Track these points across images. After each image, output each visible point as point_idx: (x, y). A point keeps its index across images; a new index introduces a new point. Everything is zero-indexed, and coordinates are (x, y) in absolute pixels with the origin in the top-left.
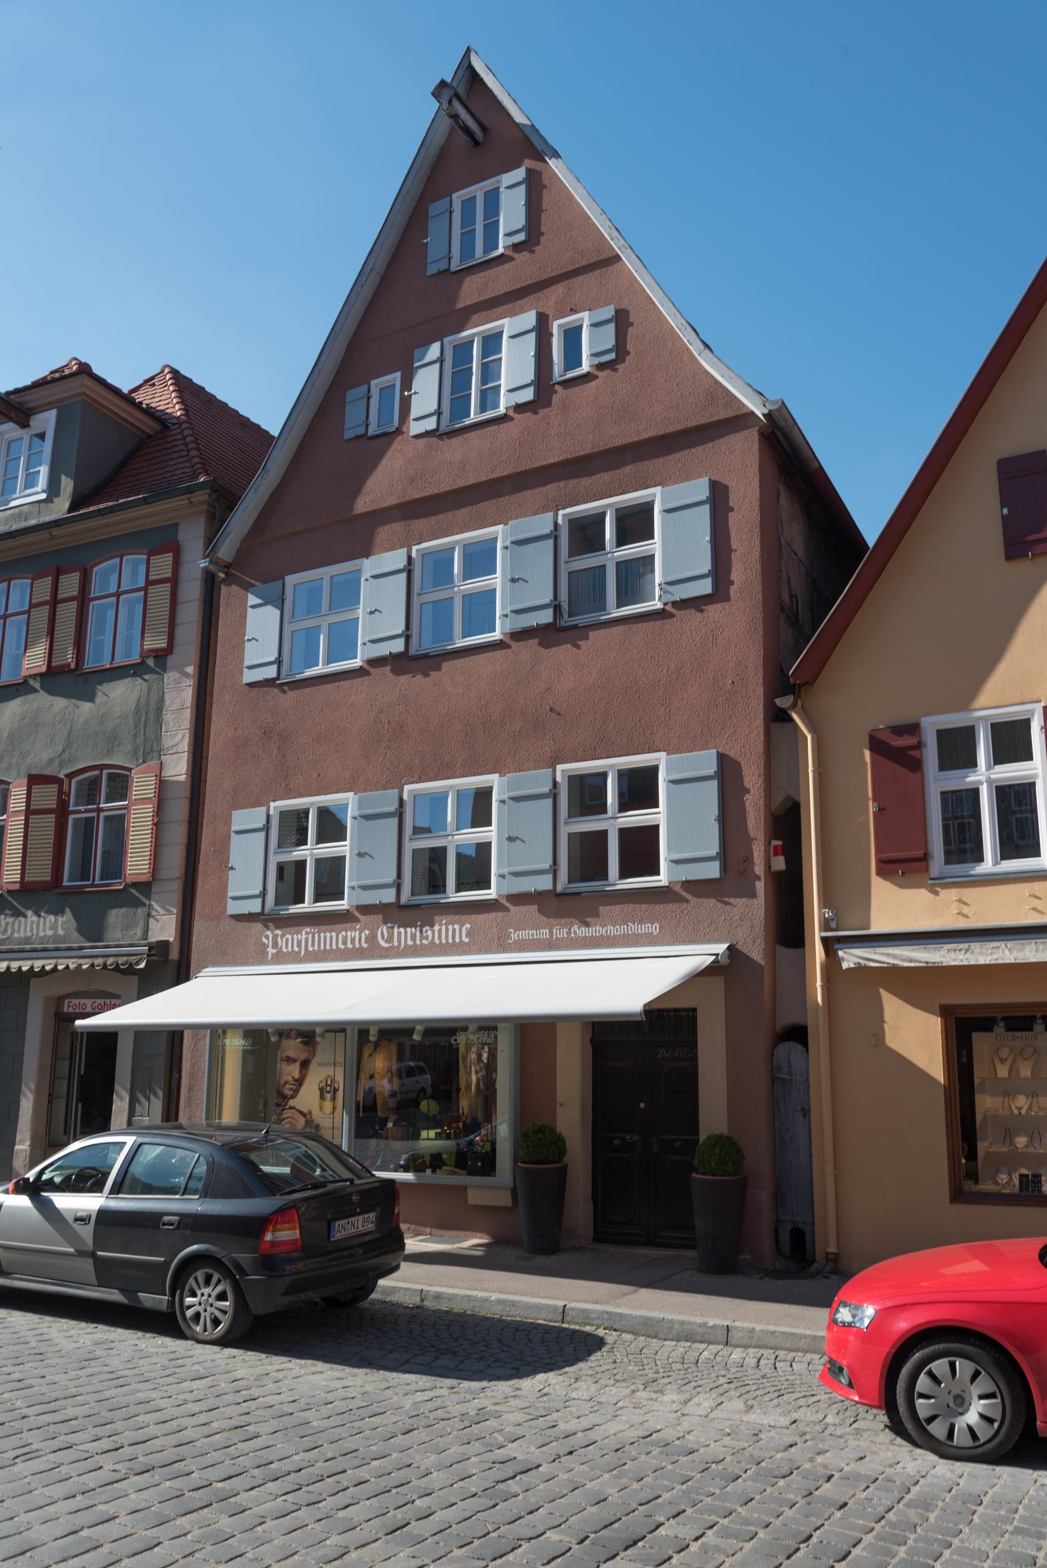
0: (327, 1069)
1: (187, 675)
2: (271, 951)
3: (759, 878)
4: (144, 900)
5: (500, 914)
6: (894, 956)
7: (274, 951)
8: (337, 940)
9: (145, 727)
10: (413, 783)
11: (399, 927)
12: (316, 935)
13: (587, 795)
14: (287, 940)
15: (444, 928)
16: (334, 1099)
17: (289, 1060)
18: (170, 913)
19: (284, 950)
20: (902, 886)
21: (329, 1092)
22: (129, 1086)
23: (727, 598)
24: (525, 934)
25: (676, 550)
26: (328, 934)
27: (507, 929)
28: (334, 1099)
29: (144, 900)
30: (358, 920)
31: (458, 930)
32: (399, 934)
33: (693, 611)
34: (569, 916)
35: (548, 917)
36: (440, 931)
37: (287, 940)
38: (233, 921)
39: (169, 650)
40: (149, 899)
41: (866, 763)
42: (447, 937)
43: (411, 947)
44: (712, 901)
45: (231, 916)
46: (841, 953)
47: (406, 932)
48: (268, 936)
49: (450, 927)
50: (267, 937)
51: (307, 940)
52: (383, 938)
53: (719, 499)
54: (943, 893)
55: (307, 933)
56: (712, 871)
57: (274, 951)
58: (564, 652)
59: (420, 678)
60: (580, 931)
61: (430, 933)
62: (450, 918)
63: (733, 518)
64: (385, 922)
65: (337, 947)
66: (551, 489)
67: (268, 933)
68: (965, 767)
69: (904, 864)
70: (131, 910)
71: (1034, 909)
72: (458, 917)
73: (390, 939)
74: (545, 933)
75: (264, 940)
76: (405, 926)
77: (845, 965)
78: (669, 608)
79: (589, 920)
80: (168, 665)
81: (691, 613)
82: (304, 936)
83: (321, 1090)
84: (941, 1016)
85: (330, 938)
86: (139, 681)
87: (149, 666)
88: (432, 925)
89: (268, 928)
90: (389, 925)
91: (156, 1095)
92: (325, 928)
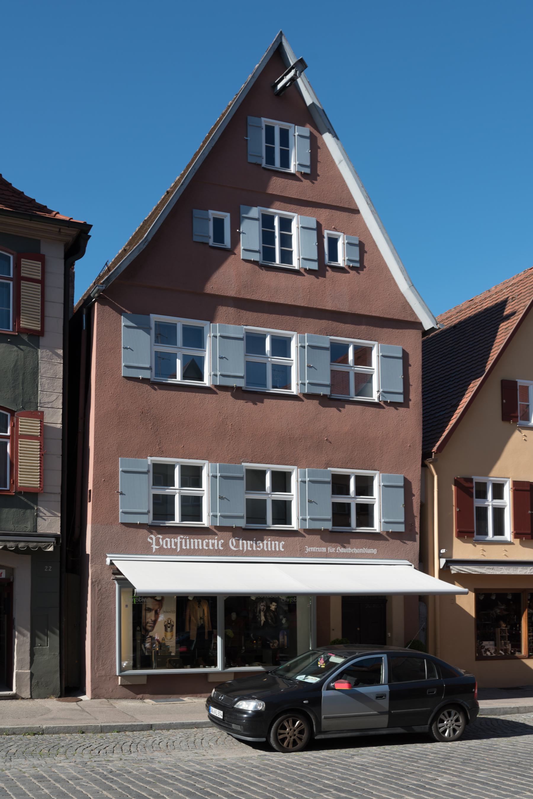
0: (166, 616)
1: (58, 355)
2: (154, 547)
3: (417, 533)
4: (32, 505)
5: (301, 538)
6: (469, 570)
7: (157, 547)
8: (202, 544)
9: (23, 384)
10: (248, 462)
11: (242, 540)
12: (188, 540)
13: (255, 479)
14: (167, 541)
15: (269, 543)
16: (172, 631)
17: (150, 610)
18: (56, 516)
19: (165, 546)
20: (464, 542)
21: (169, 627)
22: (29, 627)
23: (408, 407)
24: (314, 549)
25: (380, 376)
26: (196, 540)
27: (304, 546)
28: (172, 631)
29: (32, 505)
30: (216, 534)
31: (279, 545)
32: (243, 544)
33: (393, 408)
34: (336, 542)
35: (326, 542)
36: (267, 544)
37: (167, 541)
38: (124, 527)
39: (41, 333)
40: (37, 505)
41: (452, 491)
42: (271, 547)
43: (250, 551)
44: (399, 541)
45: (122, 523)
46: (451, 567)
47: (247, 543)
48: (152, 539)
49: (273, 542)
50: (151, 539)
51: (181, 542)
52: (233, 545)
53: (405, 357)
54: (478, 546)
55: (181, 538)
56: (401, 528)
57: (157, 547)
58: (333, 411)
59: (250, 404)
60: (342, 550)
61: (261, 544)
62: (273, 537)
63: (411, 370)
64: (234, 536)
65: (218, 548)
66: (324, 323)
67: (152, 536)
68: (483, 498)
69: (465, 534)
70: (22, 511)
71: (505, 555)
72: (277, 537)
73: (237, 546)
74: (324, 550)
75: (149, 540)
76: (246, 540)
77: (453, 572)
78: (382, 403)
79: (345, 545)
80: (41, 343)
81: (392, 409)
82: (179, 540)
83: (165, 626)
84: (474, 592)
85: (196, 542)
86: (15, 348)
87: (24, 340)
88: (262, 541)
89: (152, 533)
90: (236, 538)
91: (54, 633)
92: (194, 536)
